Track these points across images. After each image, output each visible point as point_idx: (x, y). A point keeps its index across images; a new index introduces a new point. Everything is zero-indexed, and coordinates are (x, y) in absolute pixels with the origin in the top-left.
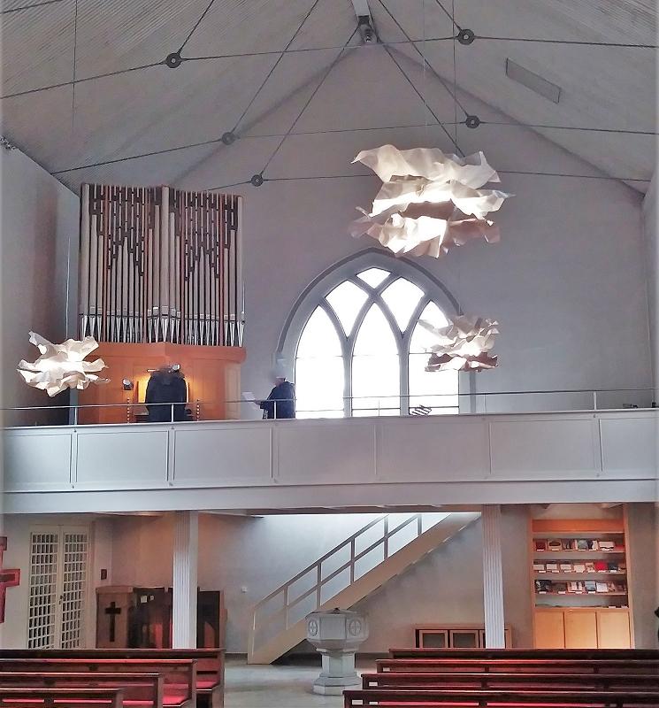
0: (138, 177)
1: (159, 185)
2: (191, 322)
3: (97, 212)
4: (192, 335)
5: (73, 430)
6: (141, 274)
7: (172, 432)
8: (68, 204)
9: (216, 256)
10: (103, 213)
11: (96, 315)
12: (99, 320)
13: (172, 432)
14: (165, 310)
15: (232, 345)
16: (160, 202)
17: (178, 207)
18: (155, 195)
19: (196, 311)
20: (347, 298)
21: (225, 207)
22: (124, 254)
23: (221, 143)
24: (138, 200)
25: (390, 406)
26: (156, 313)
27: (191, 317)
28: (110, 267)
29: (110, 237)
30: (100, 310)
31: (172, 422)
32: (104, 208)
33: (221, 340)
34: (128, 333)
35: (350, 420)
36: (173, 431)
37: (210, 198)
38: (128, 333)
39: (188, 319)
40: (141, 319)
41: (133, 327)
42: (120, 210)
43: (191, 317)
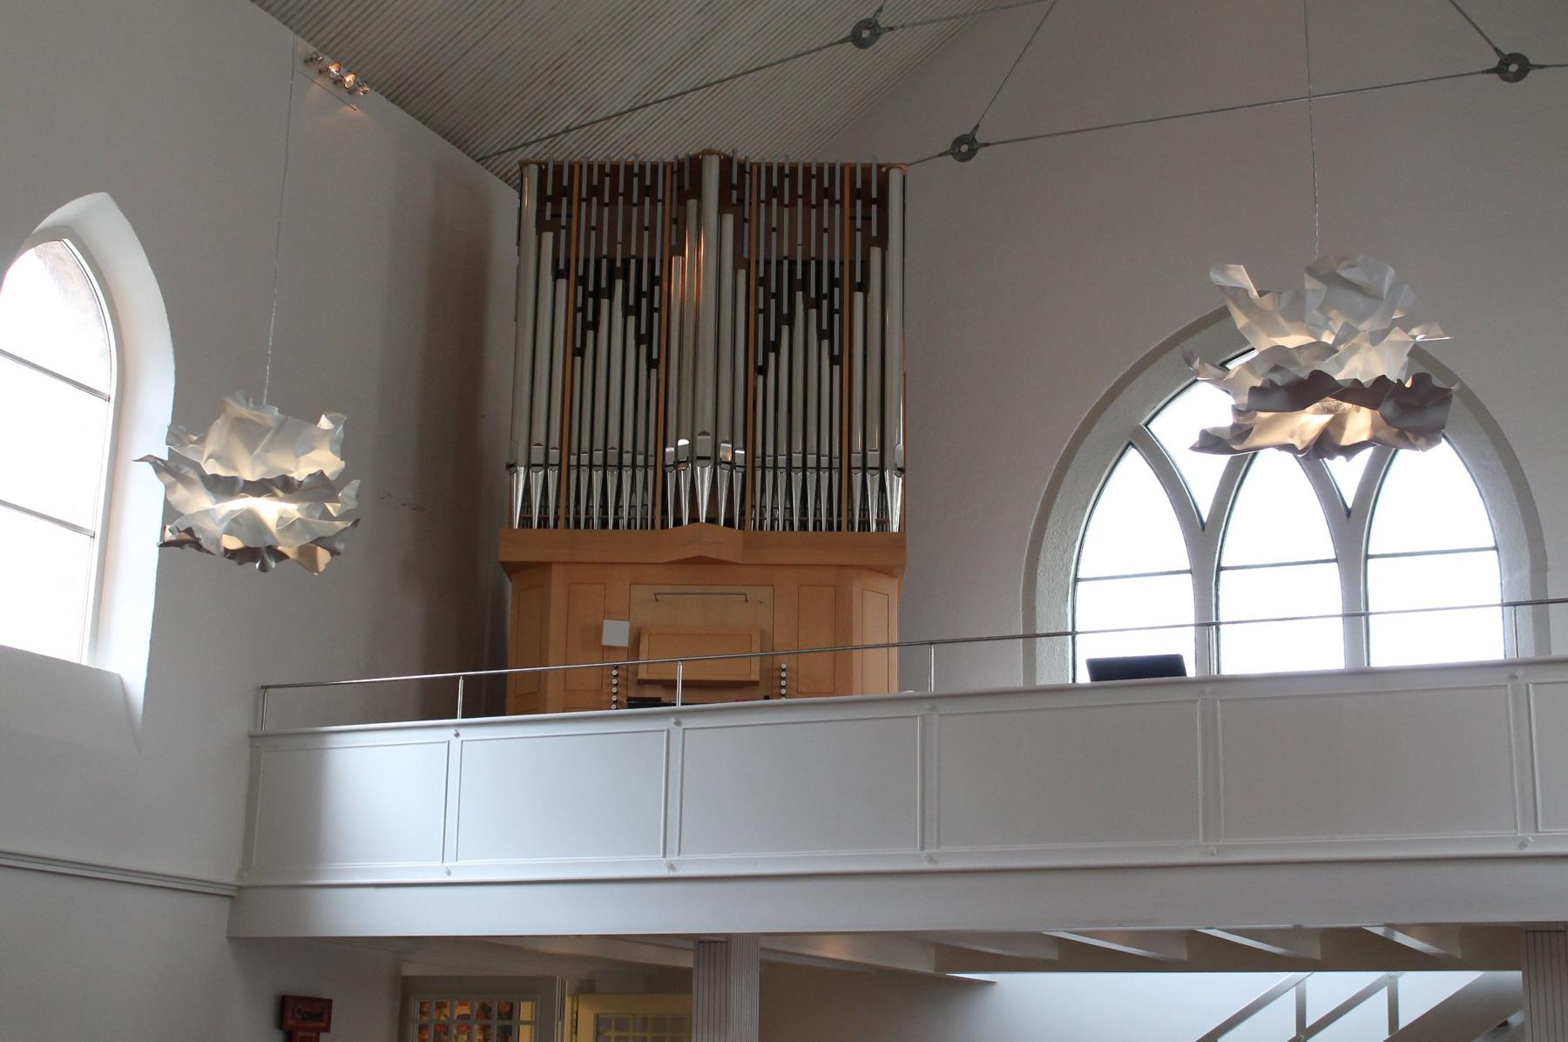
0: (656, 141)
1: (882, 159)
2: (797, 477)
3: (554, 226)
4: (774, 502)
5: (453, 731)
6: (652, 364)
7: (456, 743)
8: (508, 208)
9: (832, 312)
10: (568, 228)
11: (546, 465)
12: (553, 476)
13: (456, 743)
14: (725, 452)
15: (874, 527)
16: (697, 192)
17: (741, 200)
18: (687, 174)
19: (783, 448)
20: (1204, 406)
21: (856, 194)
22: (613, 313)
23: (850, 45)
24: (649, 191)
25: (1319, 650)
26: (669, 461)
27: (797, 460)
28: (580, 352)
29: (582, 281)
30: (554, 455)
31: (679, 707)
32: (569, 216)
33: (846, 518)
34: (617, 507)
35: (1361, 686)
36: (680, 729)
37: (641, 175)
38: (617, 507)
39: (789, 468)
40: (651, 473)
41: (632, 496)
42: (606, 222)
43: (797, 460)
